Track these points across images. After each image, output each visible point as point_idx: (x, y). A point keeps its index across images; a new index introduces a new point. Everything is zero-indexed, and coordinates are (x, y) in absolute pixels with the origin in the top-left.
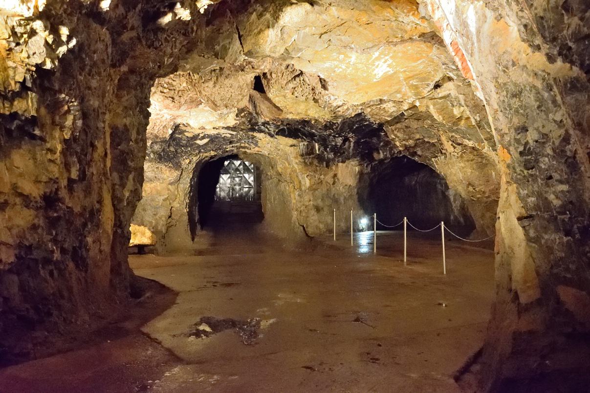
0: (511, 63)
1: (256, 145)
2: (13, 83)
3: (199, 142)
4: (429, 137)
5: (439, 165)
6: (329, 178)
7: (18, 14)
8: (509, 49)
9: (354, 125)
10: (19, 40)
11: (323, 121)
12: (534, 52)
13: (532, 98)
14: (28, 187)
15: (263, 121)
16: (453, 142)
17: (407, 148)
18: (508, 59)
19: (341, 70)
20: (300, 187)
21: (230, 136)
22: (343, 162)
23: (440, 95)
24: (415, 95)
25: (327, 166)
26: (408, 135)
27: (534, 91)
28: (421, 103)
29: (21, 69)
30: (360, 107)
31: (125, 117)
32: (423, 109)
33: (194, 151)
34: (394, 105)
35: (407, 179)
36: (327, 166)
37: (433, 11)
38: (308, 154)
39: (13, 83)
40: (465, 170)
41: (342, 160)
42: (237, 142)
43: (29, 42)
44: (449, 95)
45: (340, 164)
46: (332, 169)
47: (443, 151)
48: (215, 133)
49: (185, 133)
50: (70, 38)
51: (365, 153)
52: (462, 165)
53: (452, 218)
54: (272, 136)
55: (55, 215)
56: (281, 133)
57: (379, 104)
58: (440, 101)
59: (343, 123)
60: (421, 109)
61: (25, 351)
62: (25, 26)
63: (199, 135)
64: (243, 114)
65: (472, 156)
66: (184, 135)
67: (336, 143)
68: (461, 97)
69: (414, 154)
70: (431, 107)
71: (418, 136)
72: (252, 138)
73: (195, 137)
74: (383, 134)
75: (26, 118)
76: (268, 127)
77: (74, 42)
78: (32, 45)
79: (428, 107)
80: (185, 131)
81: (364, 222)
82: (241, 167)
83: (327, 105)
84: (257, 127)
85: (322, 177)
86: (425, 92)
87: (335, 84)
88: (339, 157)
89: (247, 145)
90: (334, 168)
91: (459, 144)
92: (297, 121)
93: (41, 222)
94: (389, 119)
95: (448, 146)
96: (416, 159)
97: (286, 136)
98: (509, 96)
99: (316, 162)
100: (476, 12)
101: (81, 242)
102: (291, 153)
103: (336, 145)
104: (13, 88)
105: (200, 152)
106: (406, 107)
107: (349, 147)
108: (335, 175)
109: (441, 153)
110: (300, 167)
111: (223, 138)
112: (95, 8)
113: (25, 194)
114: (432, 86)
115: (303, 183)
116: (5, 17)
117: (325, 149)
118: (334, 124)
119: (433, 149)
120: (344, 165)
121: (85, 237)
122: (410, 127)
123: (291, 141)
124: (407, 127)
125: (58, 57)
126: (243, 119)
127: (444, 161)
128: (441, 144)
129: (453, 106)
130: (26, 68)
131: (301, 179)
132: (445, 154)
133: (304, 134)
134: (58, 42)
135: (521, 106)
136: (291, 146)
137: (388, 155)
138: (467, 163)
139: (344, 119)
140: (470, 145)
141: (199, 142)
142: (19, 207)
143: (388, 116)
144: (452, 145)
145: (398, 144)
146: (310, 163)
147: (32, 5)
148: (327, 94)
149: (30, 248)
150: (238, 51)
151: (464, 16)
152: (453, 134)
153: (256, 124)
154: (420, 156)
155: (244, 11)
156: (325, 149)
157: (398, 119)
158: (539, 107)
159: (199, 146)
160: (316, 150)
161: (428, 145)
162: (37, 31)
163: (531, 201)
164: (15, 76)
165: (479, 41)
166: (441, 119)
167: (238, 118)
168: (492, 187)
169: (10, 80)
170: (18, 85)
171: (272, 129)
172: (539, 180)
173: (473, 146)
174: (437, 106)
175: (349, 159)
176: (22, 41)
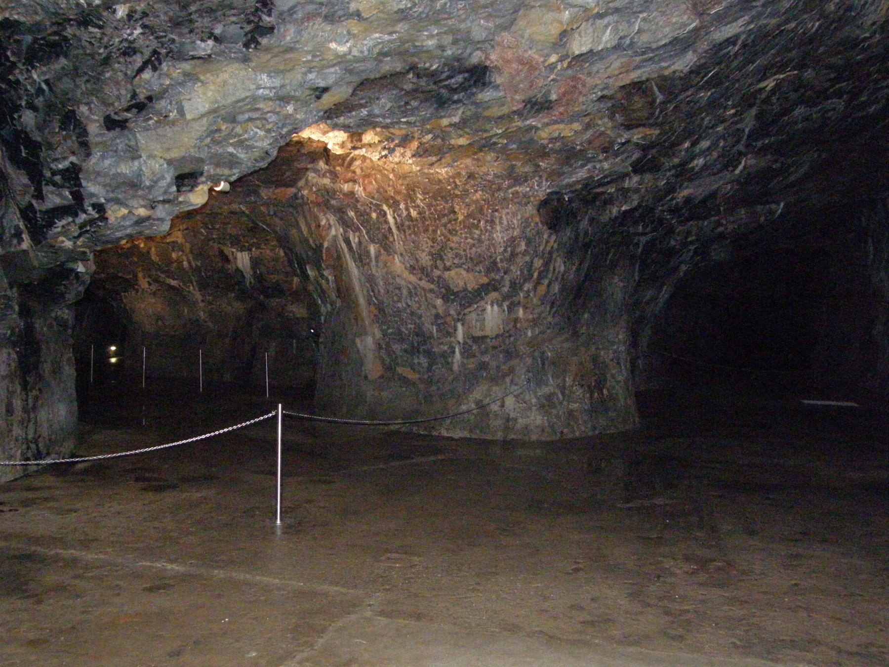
70: (153, 249)
95: (144, 283)
165: (377, 261)
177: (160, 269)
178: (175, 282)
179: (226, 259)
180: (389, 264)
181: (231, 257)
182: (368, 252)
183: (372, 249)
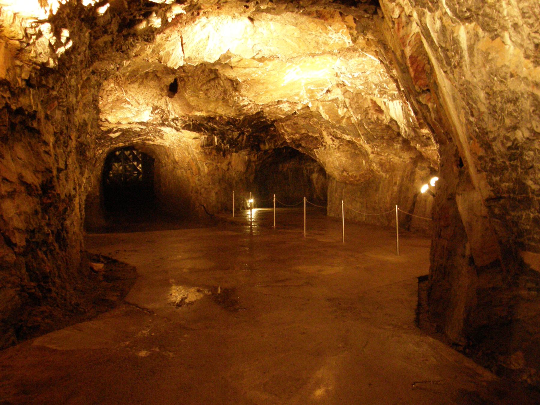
0: (509, 75)
1: (162, 138)
2: (19, 80)
3: (112, 135)
4: (313, 132)
5: (320, 154)
6: (224, 166)
7: (33, 16)
8: (507, 64)
9: (253, 122)
10: (29, 41)
11: (226, 118)
12: (535, 67)
13: (528, 103)
14: (30, 178)
15: (173, 117)
16: (333, 136)
17: (293, 141)
18: (506, 71)
19: (257, 75)
20: (199, 172)
21: (139, 130)
22: (236, 152)
23: (329, 99)
24: (310, 98)
25: (224, 155)
26: (295, 130)
27: (531, 97)
28: (313, 104)
29: (27, 67)
30: (261, 107)
31: (84, 113)
32: (313, 109)
33: (107, 143)
34: (289, 105)
35: (280, 166)
36: (224, 155)
37: (399, 29)
38: (208, 145)
39: (19, 80)
40: (341, 158)
41: (236, 150)
42: (144, 135)
43: (36, 42)
44: (337, 99)
45: (234, 154)
46: (227, 158)
47: (324, 144)
48: (127, 127)
49: (101, 128)
50: (68, 39)
51: (254, 144)
52: (338, 154)
53: (315, 196)
54: (177, 130)
55: (49, 201)
56: (187, 127)
57: (276, 105)
58: (328, 103)
59: (245, 119)
60: (312, 110)
61: (36, 324)
62: (35, 28)
63: (113, 129)
64: (156, 112)
65: (347, 148)
66: (100, 129)
67: (233, 136)
68: (347, 101)
69: (300, 145)
70: (321, 108)
71: (303, 131)
72: (159, 132)
73: (110, 131)
74: (272, 129)
75: (29, 113)
76: (177, 122)
77: (70, 44)
78: (39, 45)
79: (318, 107)
80: (101, 126)
81: (251, 201)
82: (131, 156)
83: (236, 104)
84: (166, 123)
85: (219, 164)
86: (319, 96)
87: (248, 87)
88: (233, 147)
89: (152, 138)
90: (229, 157)
91: (337, 138)
92: (204, 118)
93: (39, 208)
94: (283, 117)
95: (328, 139)
96: (300, 149)
97: (191, 130)
98: (503, 101)
99: (214, 152)
100: (468, 32)
101: (62, 225)
102: (193, 144)
103: (232, 138)
104: (21, 85)
105: (112, 143)
106: (299, 107)
107: (243, 140)
108: (230, 163)
109: (322, 145)
110: (200, 156)
111: (133, 132)
112: (91, 14)
113: (29, 183)
114: (325, 91)
115: (202, 169)
116: (21, 19)
117: (223, 142)
118: (236, 120)
119: (315, 142)
120: (237, 154)
121: (65, 220)
122: (297, 124)
123: (194, 134)
124: (295, 124)
125: (57, 57)
126: (157, 116)
127: (323, 151)
128: (323, 138)
129: (338, 107)
130: (32, 67)
131: (200, 165)
132: (325, 146)
133: (206, 129)
134: (59, 44)
135: (515, 110)
136: (194, 138)
137: (273, 147)
138: (342, 153)
139: (245, 117)
140: (348, 139)
141: (112, 135)
142: (24, 194)
143: (283, 115)
144: (331, 138)
145: (286, 137)
146: (209, 153)
147: (48, 9)
148: (237, 96)
149: (33, 232)
150: (180, 57)
151: (455, 35)
152: (335, 130)
153: (167, 120)
154: (304, 147)
155: (192, 22)
156: (223, 142)
157: (289, 117)
158: (534, 111)
159: (112, 138)
160: (215, 142)
161: (311, 138)
162: (43, 33)
163: (505, 186)
164: (21, 74)
165: (471, 55)
166: (328, 117)
167: (152, 115)
168: (363, 172)
169: (17, 77)
170: (24, 83)
171: (179, 124)
172: (519, 169)
173: (351, 139)
174: (325, 107)
175: (241, 149)
176: (31, 41)
177: (333, 126)
178: (349, 137)
179: (380, 110)
180: (493, 55)
181: (383, 108)
182: (456, 42)
183: (462, 33)
